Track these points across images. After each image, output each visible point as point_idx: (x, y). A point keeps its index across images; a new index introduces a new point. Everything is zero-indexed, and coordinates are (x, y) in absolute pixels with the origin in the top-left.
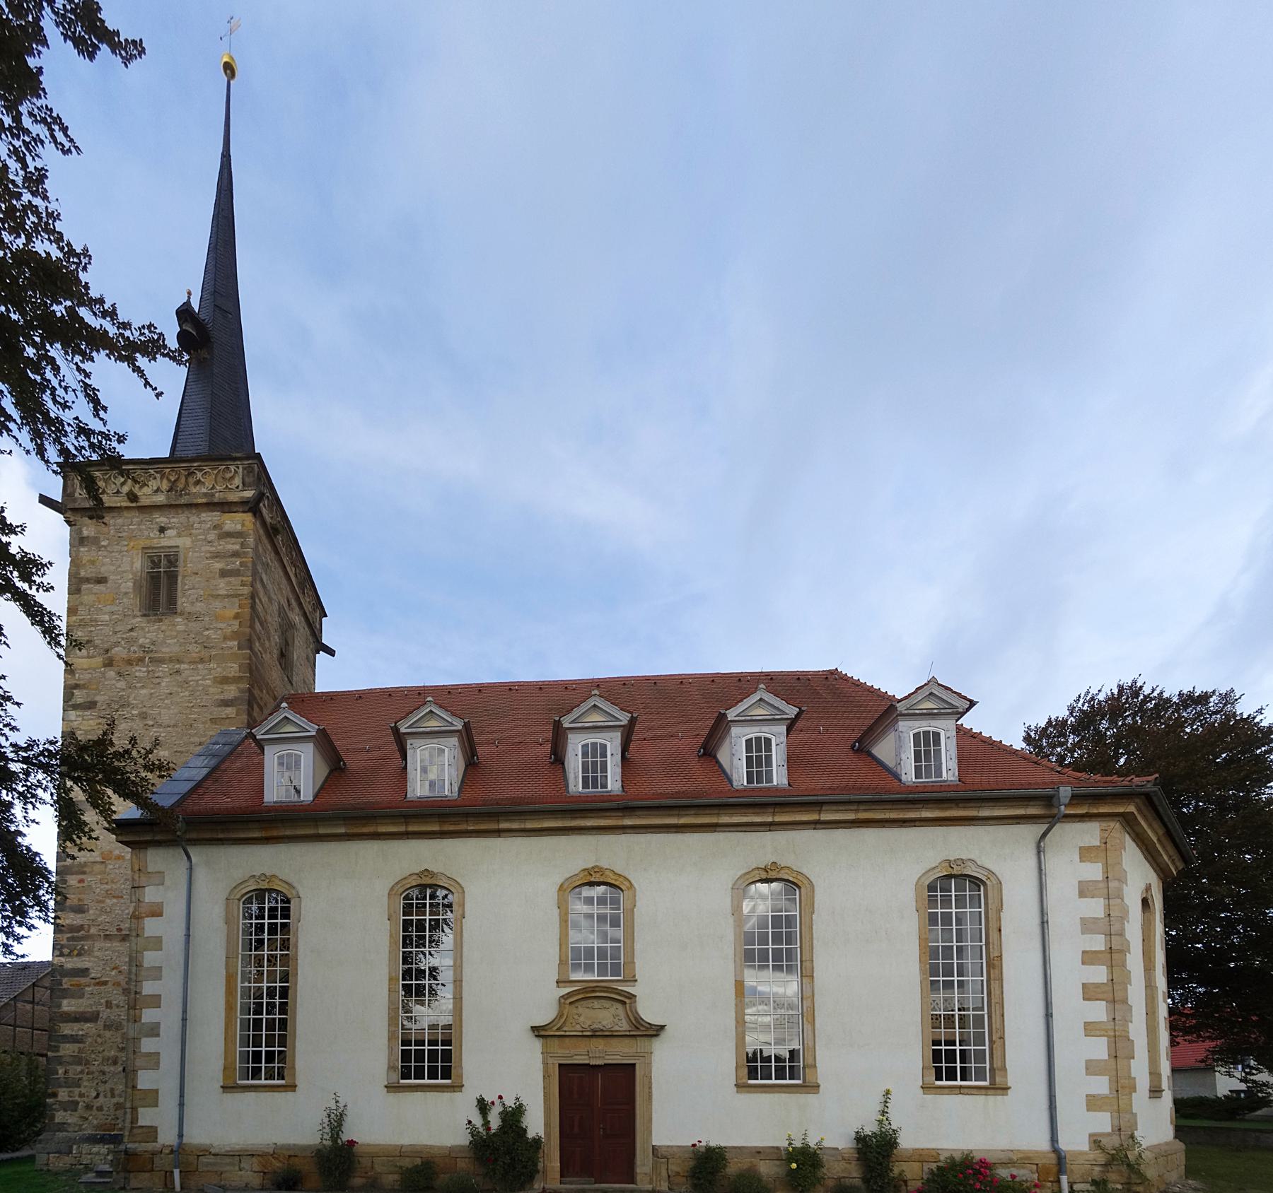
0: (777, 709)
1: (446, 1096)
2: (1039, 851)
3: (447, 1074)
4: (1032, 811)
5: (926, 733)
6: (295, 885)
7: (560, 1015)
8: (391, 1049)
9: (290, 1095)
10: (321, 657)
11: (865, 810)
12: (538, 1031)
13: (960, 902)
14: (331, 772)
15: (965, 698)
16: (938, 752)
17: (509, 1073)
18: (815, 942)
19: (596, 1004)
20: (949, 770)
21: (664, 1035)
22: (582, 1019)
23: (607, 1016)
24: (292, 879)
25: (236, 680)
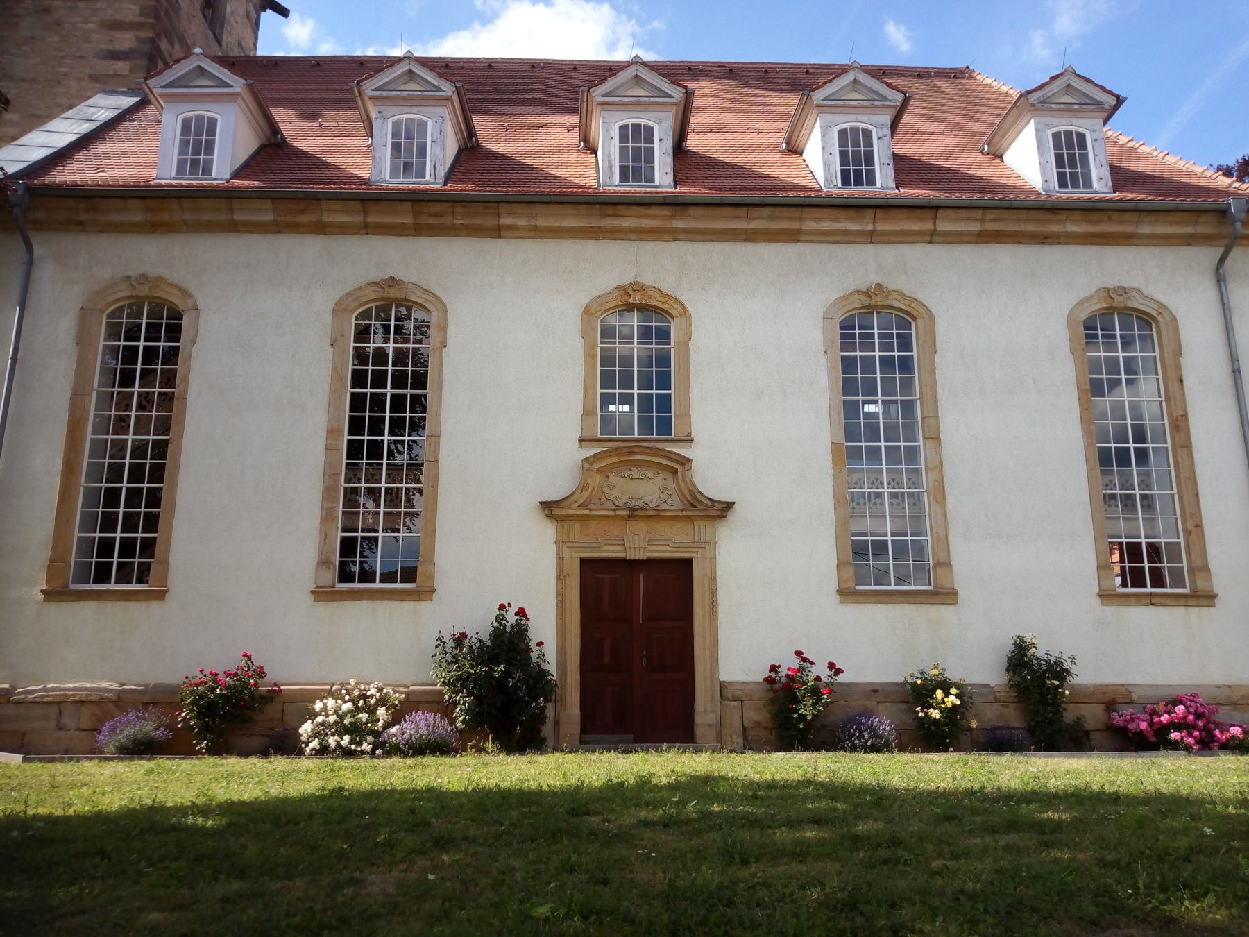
0: (877, 93)
1: (407, 607)
2: (1220, 279)
3: (409, 574)
4: (1202, 229)
5: (1068, 134)
6: (193, 291)
7: (584, 487)
8: (325, 536)
9: (155, 606)
10: (268, 16)
11: (995, 220)
12: (549, 508)
13: (1127, 343)
14: (262, 148)
15: (1110, 93)
16: (1084, 158)
17: (500, 556)
18: (940, 391)
19: (635, 473)
20: (1100, 184)
21: (732, 517)
22: (615, 493)
23: (648, 489)
24: (190, 283)
25: (132, 26)
